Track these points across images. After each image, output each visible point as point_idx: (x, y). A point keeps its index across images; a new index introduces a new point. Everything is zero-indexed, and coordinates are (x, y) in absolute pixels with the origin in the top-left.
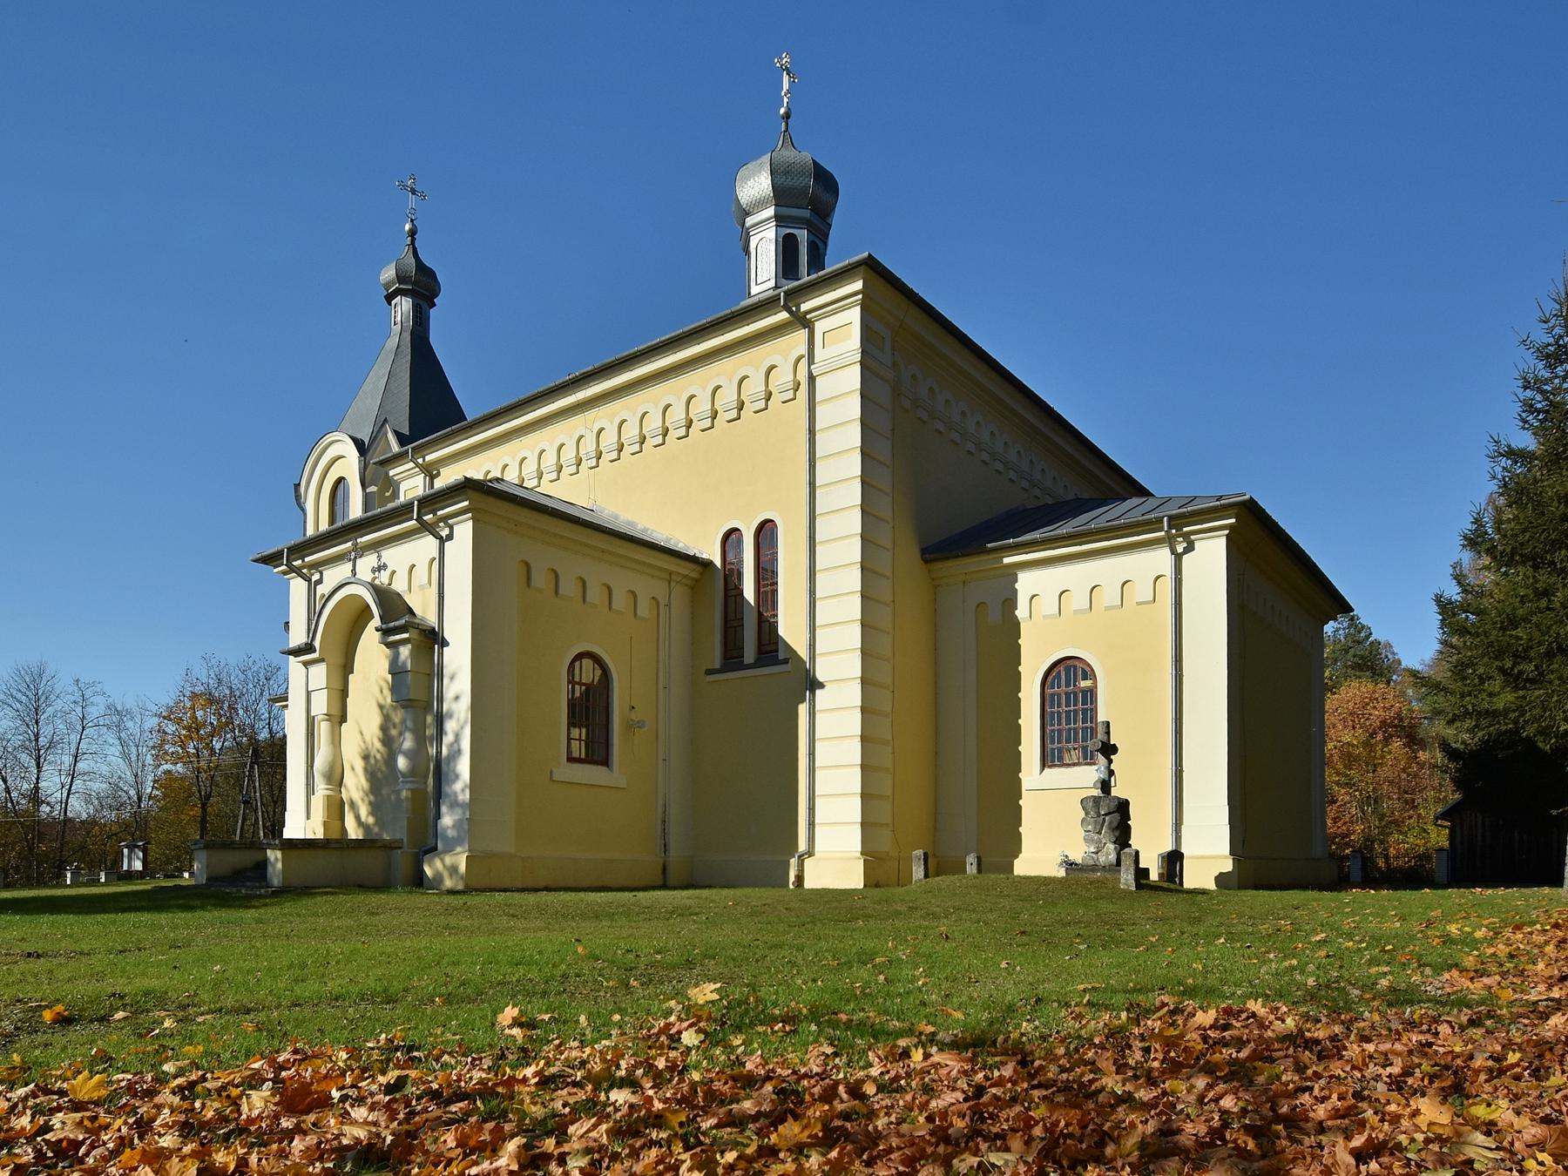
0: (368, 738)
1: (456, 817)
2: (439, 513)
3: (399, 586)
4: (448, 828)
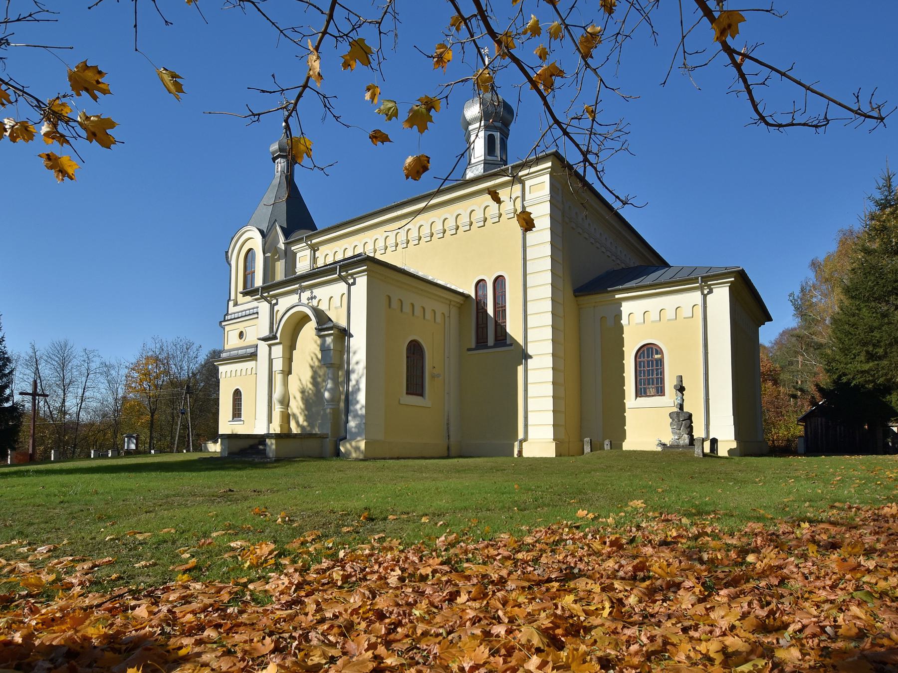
0: (304, 383)
1: (357, 423)
2: (349, 272)
3: (323, 307)
4: (352, 427)
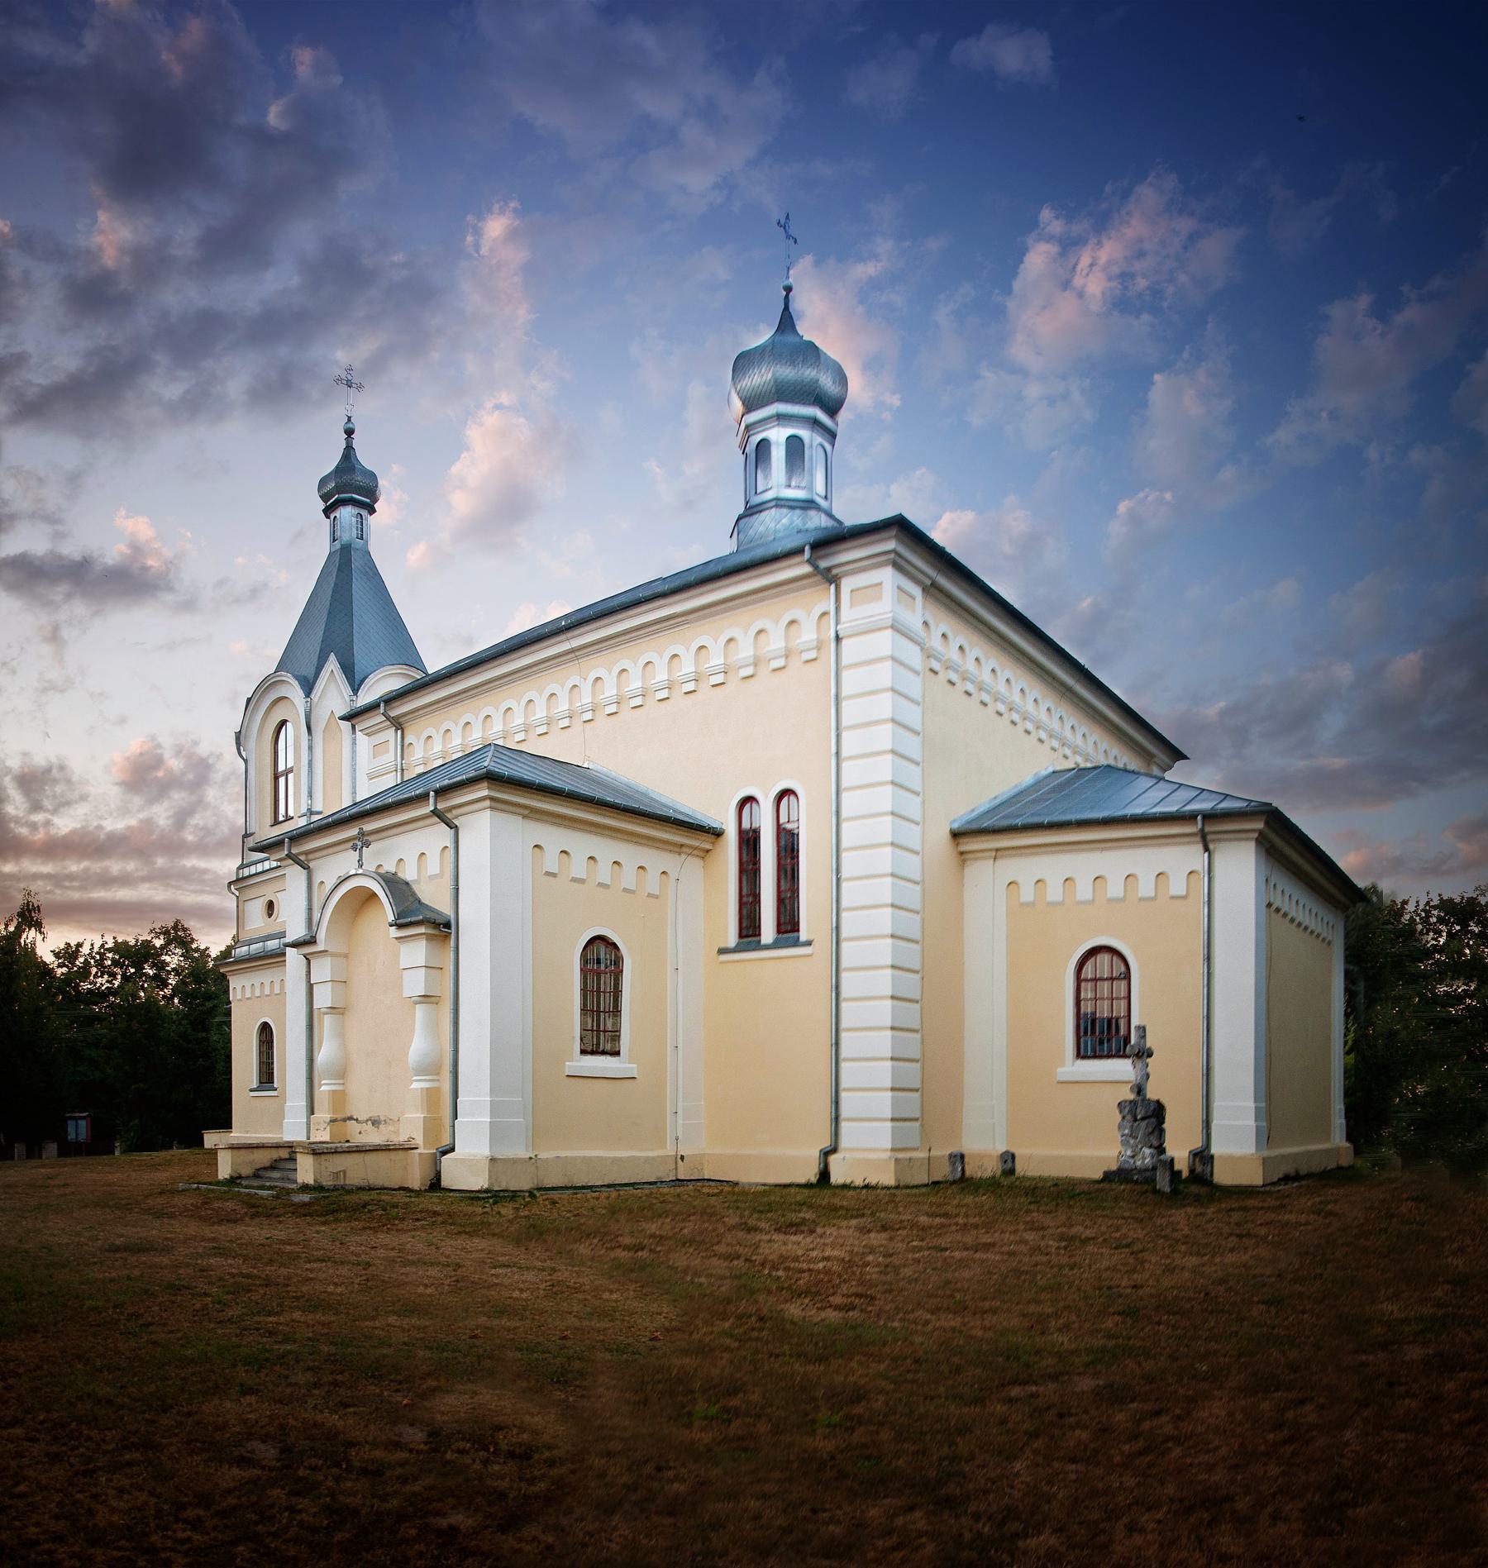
3: (409, 874)
